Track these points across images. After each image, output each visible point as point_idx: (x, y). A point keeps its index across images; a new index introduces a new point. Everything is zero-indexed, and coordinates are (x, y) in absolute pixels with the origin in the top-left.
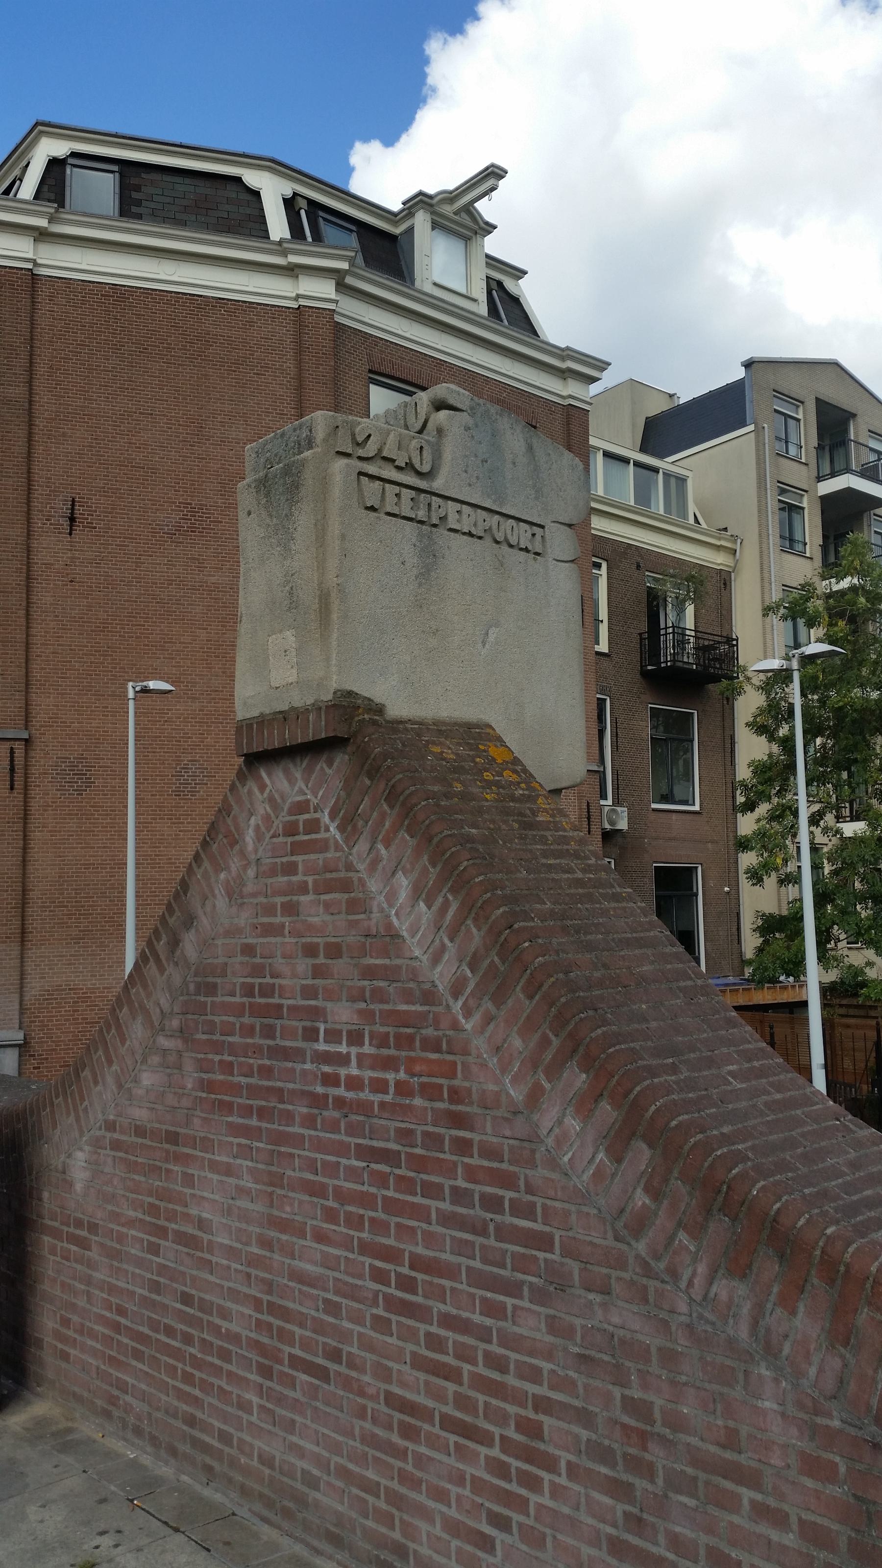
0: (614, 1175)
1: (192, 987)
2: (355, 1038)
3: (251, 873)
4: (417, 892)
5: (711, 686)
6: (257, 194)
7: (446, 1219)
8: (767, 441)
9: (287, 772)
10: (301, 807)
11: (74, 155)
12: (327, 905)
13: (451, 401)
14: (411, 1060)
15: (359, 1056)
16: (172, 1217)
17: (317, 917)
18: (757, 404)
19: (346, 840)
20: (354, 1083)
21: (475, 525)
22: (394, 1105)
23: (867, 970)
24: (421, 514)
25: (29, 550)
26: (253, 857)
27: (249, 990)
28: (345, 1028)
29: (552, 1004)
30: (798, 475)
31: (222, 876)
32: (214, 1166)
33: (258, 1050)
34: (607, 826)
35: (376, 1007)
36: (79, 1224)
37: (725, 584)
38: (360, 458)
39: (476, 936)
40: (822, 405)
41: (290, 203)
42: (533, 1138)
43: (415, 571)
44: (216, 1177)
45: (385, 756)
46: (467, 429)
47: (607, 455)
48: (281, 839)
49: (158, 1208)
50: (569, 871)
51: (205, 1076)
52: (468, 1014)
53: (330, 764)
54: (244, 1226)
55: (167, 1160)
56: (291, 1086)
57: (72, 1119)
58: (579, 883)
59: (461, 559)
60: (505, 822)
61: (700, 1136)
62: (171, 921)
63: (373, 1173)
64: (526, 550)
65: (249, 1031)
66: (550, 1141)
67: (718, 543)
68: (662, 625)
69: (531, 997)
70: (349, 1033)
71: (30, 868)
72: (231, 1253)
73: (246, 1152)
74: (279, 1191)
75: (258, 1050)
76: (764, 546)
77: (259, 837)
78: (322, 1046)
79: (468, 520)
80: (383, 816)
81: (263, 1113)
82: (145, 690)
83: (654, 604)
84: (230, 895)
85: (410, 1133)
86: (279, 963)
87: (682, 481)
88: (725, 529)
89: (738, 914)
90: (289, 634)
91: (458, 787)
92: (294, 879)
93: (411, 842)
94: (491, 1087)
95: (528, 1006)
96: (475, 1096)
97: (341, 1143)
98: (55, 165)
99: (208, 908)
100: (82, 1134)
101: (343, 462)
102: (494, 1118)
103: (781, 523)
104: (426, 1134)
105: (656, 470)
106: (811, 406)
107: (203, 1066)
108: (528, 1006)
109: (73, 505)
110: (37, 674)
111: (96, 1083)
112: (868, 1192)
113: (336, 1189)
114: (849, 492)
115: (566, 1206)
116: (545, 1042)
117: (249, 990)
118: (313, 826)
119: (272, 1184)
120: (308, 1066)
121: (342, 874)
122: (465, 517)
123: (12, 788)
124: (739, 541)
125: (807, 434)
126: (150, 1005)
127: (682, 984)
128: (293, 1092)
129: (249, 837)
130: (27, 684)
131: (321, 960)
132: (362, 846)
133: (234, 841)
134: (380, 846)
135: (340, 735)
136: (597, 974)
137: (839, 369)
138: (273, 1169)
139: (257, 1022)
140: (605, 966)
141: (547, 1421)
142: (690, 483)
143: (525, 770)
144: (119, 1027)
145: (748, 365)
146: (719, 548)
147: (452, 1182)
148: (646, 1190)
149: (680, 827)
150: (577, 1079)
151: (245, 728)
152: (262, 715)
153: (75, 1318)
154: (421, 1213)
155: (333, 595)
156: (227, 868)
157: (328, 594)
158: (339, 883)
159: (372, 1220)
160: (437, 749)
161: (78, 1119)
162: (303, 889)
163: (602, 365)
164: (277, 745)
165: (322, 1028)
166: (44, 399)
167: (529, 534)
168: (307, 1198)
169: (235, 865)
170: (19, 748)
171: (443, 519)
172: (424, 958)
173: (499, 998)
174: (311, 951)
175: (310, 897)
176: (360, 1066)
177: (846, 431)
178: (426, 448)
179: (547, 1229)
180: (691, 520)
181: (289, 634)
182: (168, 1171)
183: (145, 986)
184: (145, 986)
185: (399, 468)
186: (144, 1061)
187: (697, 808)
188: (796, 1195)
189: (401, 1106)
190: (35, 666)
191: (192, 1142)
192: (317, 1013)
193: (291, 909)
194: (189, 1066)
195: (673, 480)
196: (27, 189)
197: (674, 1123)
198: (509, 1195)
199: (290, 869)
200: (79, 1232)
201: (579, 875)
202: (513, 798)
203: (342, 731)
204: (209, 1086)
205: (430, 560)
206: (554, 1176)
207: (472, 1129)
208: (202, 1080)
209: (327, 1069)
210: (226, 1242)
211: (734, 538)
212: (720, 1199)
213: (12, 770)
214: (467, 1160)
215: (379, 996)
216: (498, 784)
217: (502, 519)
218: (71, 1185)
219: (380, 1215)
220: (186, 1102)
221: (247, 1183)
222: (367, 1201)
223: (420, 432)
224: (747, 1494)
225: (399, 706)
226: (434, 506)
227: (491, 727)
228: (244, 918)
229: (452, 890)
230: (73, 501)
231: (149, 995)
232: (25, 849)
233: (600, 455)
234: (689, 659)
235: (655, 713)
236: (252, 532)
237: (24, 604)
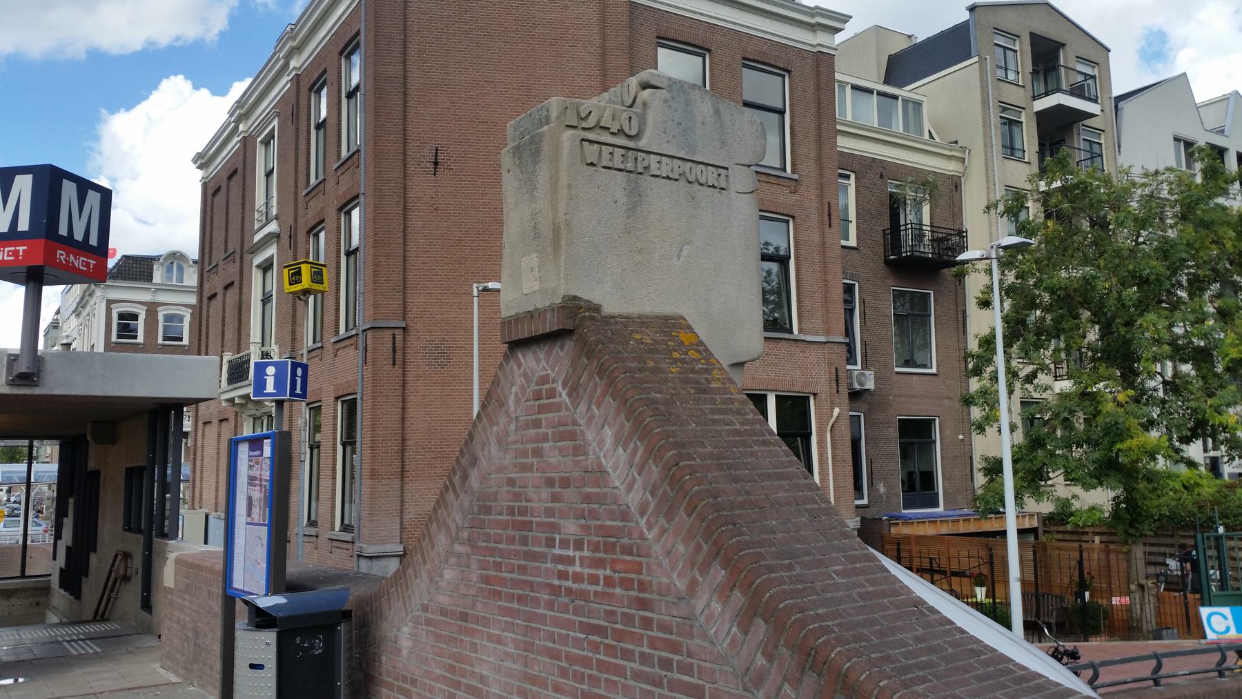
0: (743, 643)
1: (476, 509)
2: (579, 545)
3: (513, 427)
4: (617, 440)
5: (945, 271)
7: (637, 676)
9: (535, 354)
10: (544, 380)
12: (561, 450)
13: (653, 82)
14: (614, 561)
15: (581, 558)
17: (554, 459)
18: (977, 39)
19: (572, 403)
20: (578, 578)
21: (672, 170)
22: (603, 593)
23: (1073, 501)
24: (630, 166)
25: (405, 187)
26: (513, 416)
27: (511, 512)
28: (572, 538)
29: (703, 520)
30: (1016, 96)
31: (495, 429)
32: (490, 637)
33: (517, 554)
34: (857, 387)
35: (592, 523)
36: (405, 679)
38: (584, 129)
39: (655, 471)
40: (1036, 39)
42: (690, 618)
43: (625, 207)
44: (491, 645)
45: (598, 342)
46: (666, 101)
47: (854, 87)
48: (532, 403)
49: (454, 667)
50: (730, 423)
51: (484, 572)
52: (650, 528)
53: (562, 348)
54: (508, 680)
55: (460, 633)
56: (538, 579)
57: (401, 603)
58: (738, 433)
59: (660, 196)
60: (684, 389)
61: (799, 615)
62: (463, 461)
63: (591, 642)
64: (713, 186)
65: (511, 540)
66: (702, 619)
68: (902, 222)
69: (689, 515)
70: (575, 541)
71: (407, 423)
73: (509, 627)
74: (532, 656)
75: (517, 554)
76: (989, 154)
77: (517, 402)
78: (557, 551)
79: (667, 167)
80: (596, 385)
81: (521, 599)
82: (486, 290)
83: (895, 205)
84: (499, 443)
85: (613, 613)
86: (531, 492)
87: (918, 104)
88: (956, 142)
89: (971, 458)
90: (534, 256)
91: (651, 364)
92: (540, 431)
93: (614, 404)
94: (665, 580)
95: (688, 521)
96: (654, 587)
97: (570, 620)
99: (486, 453)
100: (407, 614)
101: (572, 132)
102: (667, 602)
103: (1003, 134)
104: (624, 614)
105: (896, 98)
107: (483, 566)
108: (688, 521)
111: (416, 577)
112: (924, 658)
113: (567, 653)
114: (1060, 108)
115: (713, 666)
116: (699, 548)
117: (511, 512)
118: (552, 393)
119: (526, 650)
120: (549, 565)
121: (569, 428)
122: (664, 165)
125: (1023, 61)
126: (450, 522)
127: (809, 506)
128: (539, 583)
129: (511, 401)
130: (404, 287)
131: (557, 489)
132: (582, 407)
134: (594, 407)
135: (569, 328)
136: (740, 499)
138: (528, 639)
139: (517, 534)
140: (748, 493)
142: (925, 105)
143: (706, 350)
144: (430, 537)
145: (972, 9)
146: (950, 157)
147: (640, 649)
148: (764, 654)
149: (920, 388)
150: (719, 574)
151: (507, 323)
152: (517, 314)
154: (619, 671)
155: (563, 227)
156: (498, 424)
157: (559, 228)
159: (590, 676)
160: (638, 336)
161: (404, 604)
162: (545, 438)
163: (845, 19)
164: (527, 335)
165: (558, 537)
166: (414, 73)
167: (715, 175)
168: (548, 660)
169: (502, 420)
170: (399, 333)
171: (647, 168)
172: (622, 488)
173: (669, 516)
174: (550, 483)
175: (550, 444)
176: (582, 565)
177: (1057, 58)
178: (634, 117)
179: (701, 682)
180: (927, 136)
181: (534, 256)
182: (461, 641)
183: (446, 508)
184: (446, 508)
185: (613, 134)
186: (446, 561)
187: (934, 370)
188: (864, 658)
189: (607, 594)
190: (410, 274)
191: (476, 619)
192: (554, 527)
193: (538, 453)
194: (474, 566)
195: (910, 105)
197: (782, 606)
198: (676, 658)
199: (537, 424)
200: (405, 685)
201: (738, 426)
202: (693, 371)
204: (487, 580)
205: (636, 199)
206: (705, 644)
207: (652, 611)
208: (482, 575)
209: (561, 567)
210: (498, 692)
211: (963, 149)
212: (810, 660)
213: (394, 351)
214: (649, 633)
215: (594, 515)
216: (682, 361)
217: (693, 165)
218: (400, 651)
219: (595, 672)
220: (472, 591)
222: (586, 662)
223: (631, 106)
225: (611, 306)
226: (640, 159)
227: (684, 318)
228: (509, 459)
229: (640, 438)
231: (449, 514)
232: (403, 409)
233: (848, 88)
234: (926, 250)
235: (898, 295)
236: (510, 184)
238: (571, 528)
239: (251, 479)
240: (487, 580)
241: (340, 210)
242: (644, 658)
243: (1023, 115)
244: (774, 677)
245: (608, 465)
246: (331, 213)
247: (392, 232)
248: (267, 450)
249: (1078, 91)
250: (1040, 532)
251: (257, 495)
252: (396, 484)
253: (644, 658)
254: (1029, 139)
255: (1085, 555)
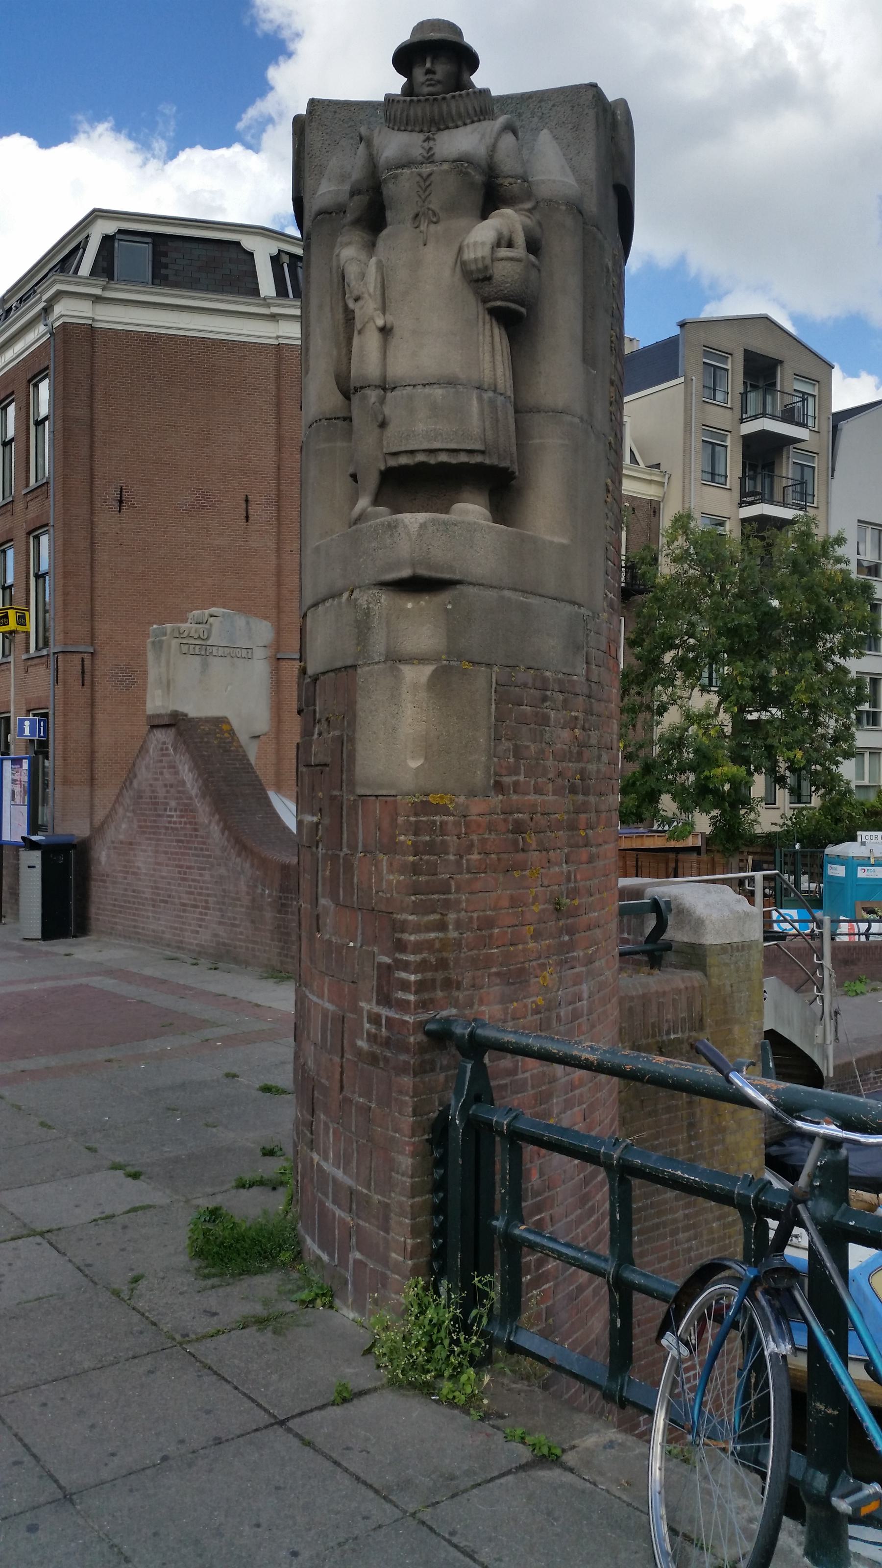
2: (175, 810)
4: (190, 770)
6: (251, 254)
7: (193, 855)
8: (694, 391)
10: (164, 743)
11: (120, 231)
16: (131, 867)
17: (167, 776)
20: (175, 823)
27: (151, 798)
30: (720, 418)
32: (142, 850)
36: (103, 875)
37: (654, 512)
39: (200, 781)
41: (275, 260)
59: (217, 665)
65: (150, 809)
67: (649, 478)
72: (146, 874)
76: (687, 481)
77: (154, 751)
78: (168, 813)
81: (154, 833)
91: (206, 740)
98: (107, 240)
101: (176, 640)
106: (740, 358)
107: (139, 821)
109: (121, 492)
110: (98, 608)
114: (764, 435)
117: (151, 798)
118: (167, 749)
123: (83, 685)
124: (667, 476)
125: (736, 379)
129: (151, 751)
132: (178, 756)
133: (147, 751)
135: (175, 722)
137: (768, 322)
141: (209, 899)
145: (682, 325)
146: (650, 482)
151: (151, 717)
153: (102, 906)
154: (188, 854)
158: (173, 767)
162: (164, 768)
169: (147, 759)
174: (166, 786)
192: (167, 804)
194: (135, 821)
196: (85, 269)
199: (161, 761)
203: (173, 722)
204: (140, 827)
205: (205, 666)
213: (83, 673)
215: (181, 798)
216: (221, 738)
221: (150, 854)
222: (177, 853)
224: (239, 903)
230: (121, 488)
232: (92, 724)
236: (150, 656)
237: (89, 561)
238: (173, 804)
239: (14, 781)
240: (140, 827)
241: (29, 533)
242: (196, 849)
243: (729, 439)
244: (229, 847)
245: (186, 779)
246: (20, 535)
247: (80, 570)
248: (25, 764)
249: (788, 416)
250: (703, 850)
251: (18, 789)
252: (87, 791)
253: (196, 849)
254: (733, 464)
255: (680, 865)
